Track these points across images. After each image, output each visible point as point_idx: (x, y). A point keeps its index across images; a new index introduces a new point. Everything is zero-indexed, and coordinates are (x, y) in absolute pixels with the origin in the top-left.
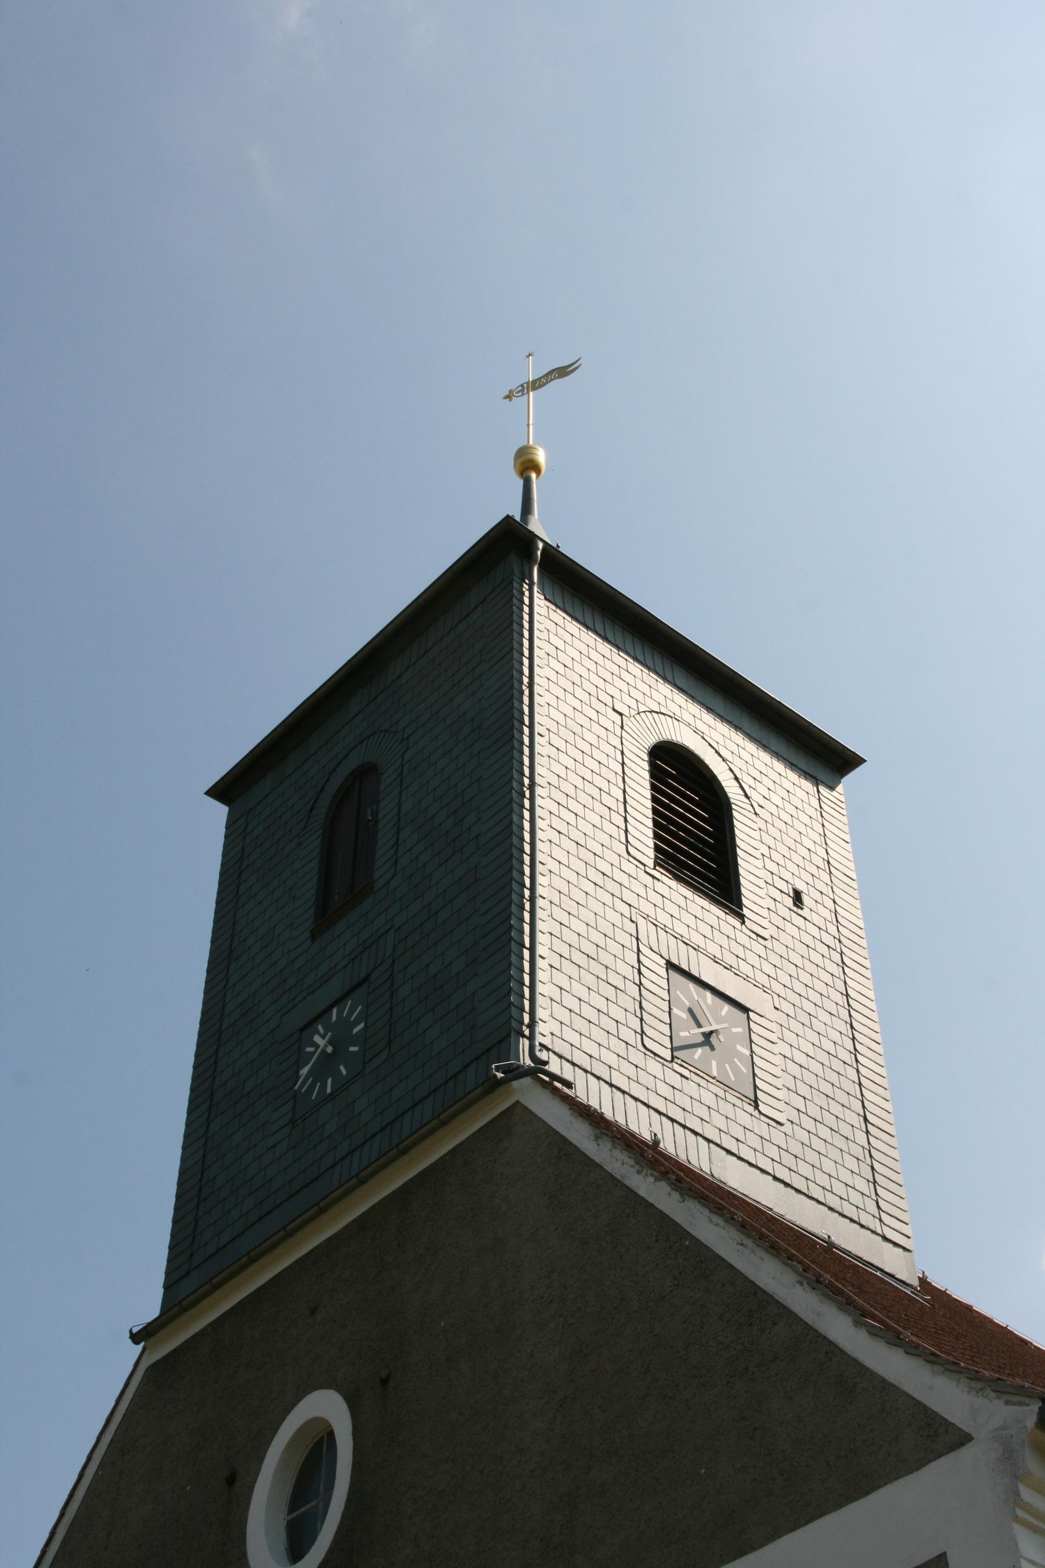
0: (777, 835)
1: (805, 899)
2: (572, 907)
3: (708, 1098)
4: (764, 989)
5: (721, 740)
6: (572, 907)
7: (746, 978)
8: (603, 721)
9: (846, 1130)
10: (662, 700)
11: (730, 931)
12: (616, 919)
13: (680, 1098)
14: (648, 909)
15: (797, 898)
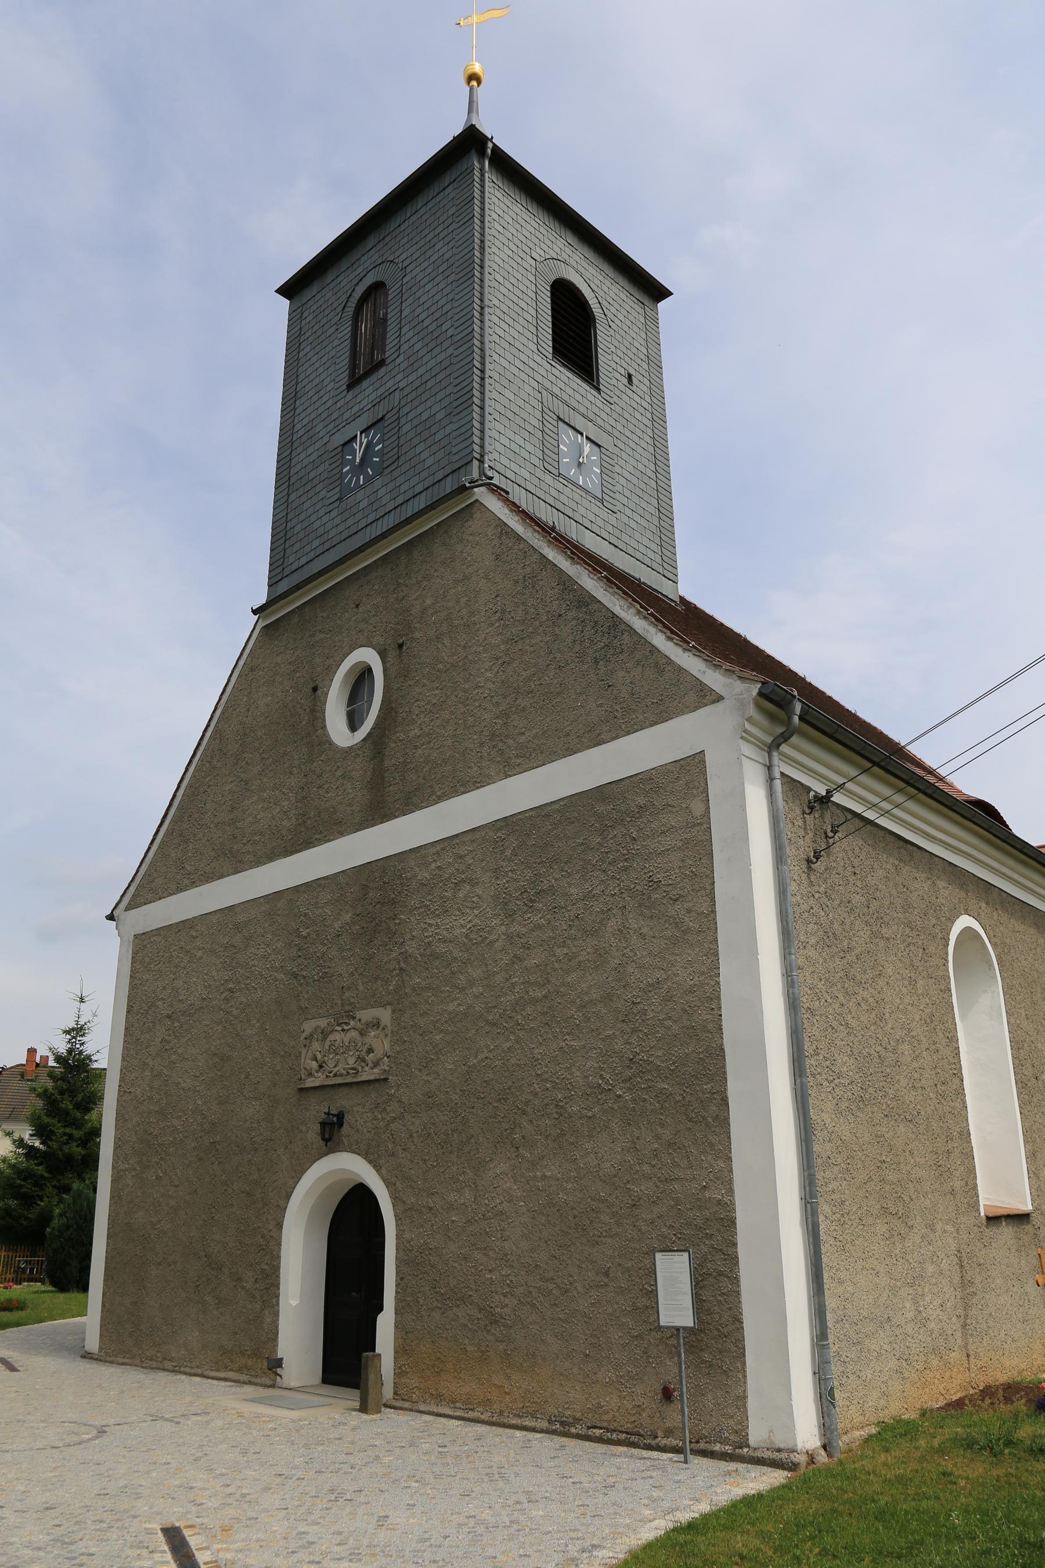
0: (620, 339)
1: (634, 379)
2: (506, 383)
3: (577, 498)
4: (609, 433)
5: (591, 277)
6: (506, 383)
7: (600, 427)
8: (525, 264)
9: (648, 516)
10: (558, 250)
11: (592, 398)
12: (530, 391)
13: (563, 498)
14: (548, 385)
15: (630, 377)
